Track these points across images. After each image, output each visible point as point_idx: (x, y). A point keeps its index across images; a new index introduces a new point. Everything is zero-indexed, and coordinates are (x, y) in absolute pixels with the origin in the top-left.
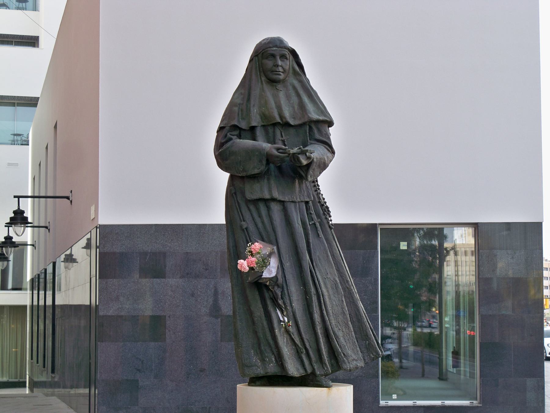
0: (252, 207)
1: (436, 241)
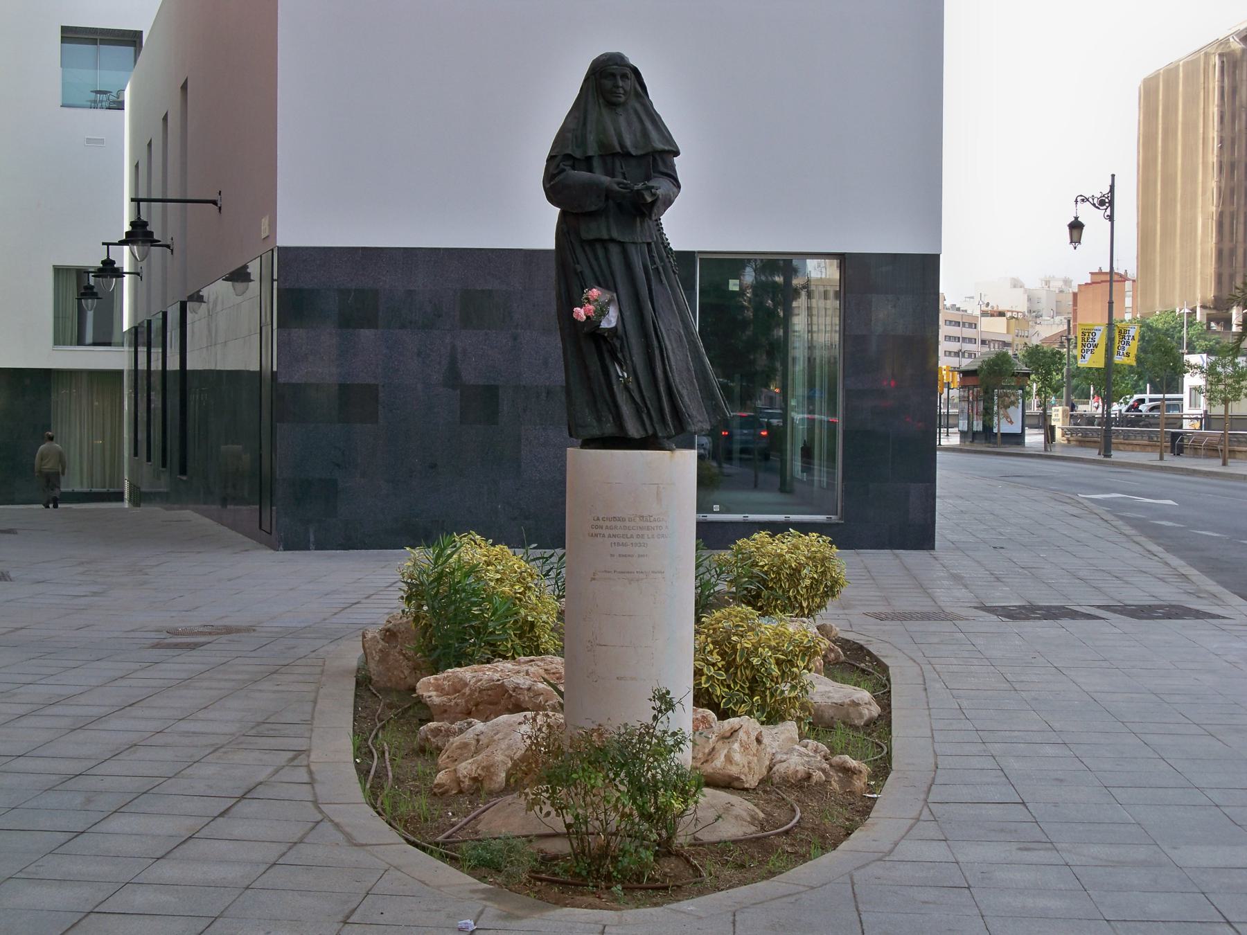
0: (587, 248)
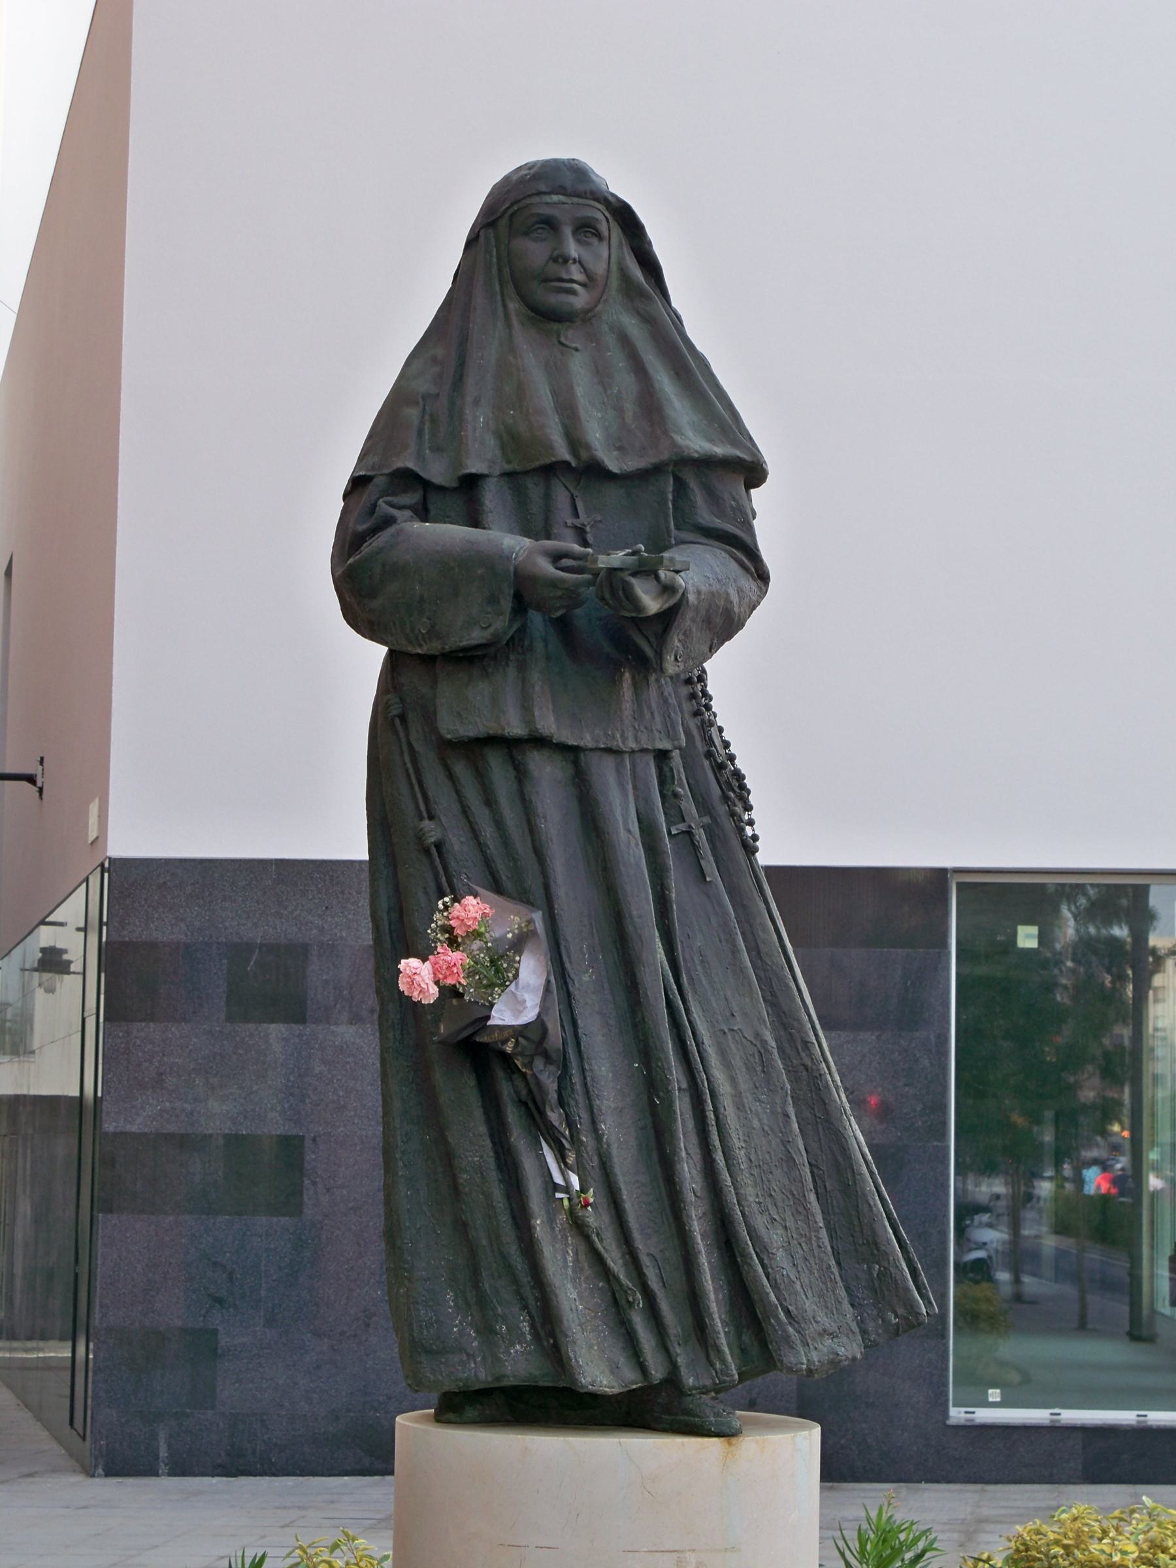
0: (461, 769)
1: (1124, 927)
